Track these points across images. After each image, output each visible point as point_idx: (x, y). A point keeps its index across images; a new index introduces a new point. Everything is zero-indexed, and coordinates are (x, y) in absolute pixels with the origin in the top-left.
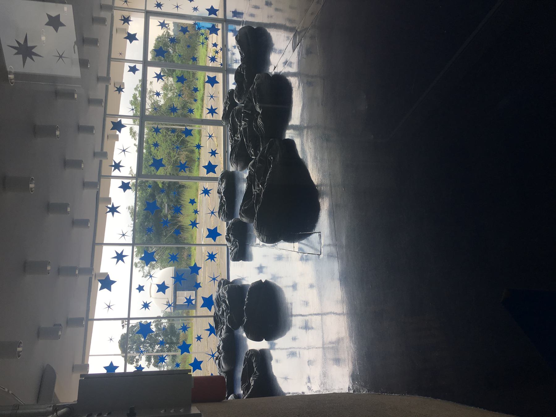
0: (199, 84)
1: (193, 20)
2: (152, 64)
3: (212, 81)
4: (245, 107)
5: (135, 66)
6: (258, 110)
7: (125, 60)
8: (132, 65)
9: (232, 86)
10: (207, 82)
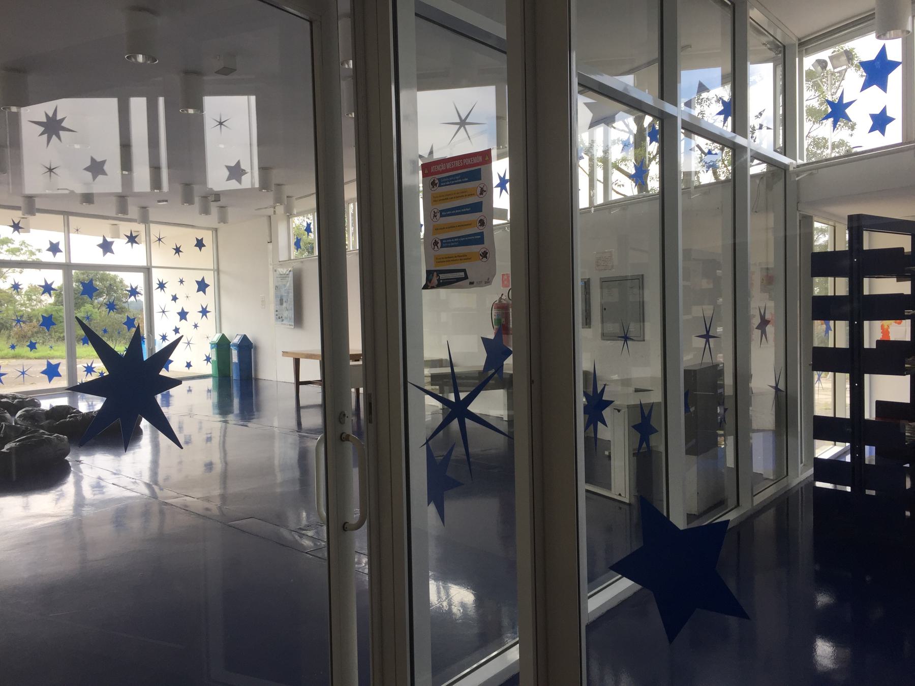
0: (42, 350)
1: (148, 335)
2: (67, 277)
3: (52, 372)
4: (10, 427)
5: (61, 251)
6: (7, 446)
7: (69, 233)
8: (62, 247)
9: (46, 405)
10: (49, 364)
